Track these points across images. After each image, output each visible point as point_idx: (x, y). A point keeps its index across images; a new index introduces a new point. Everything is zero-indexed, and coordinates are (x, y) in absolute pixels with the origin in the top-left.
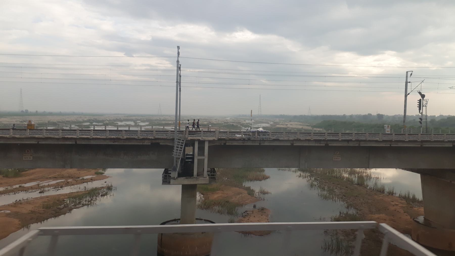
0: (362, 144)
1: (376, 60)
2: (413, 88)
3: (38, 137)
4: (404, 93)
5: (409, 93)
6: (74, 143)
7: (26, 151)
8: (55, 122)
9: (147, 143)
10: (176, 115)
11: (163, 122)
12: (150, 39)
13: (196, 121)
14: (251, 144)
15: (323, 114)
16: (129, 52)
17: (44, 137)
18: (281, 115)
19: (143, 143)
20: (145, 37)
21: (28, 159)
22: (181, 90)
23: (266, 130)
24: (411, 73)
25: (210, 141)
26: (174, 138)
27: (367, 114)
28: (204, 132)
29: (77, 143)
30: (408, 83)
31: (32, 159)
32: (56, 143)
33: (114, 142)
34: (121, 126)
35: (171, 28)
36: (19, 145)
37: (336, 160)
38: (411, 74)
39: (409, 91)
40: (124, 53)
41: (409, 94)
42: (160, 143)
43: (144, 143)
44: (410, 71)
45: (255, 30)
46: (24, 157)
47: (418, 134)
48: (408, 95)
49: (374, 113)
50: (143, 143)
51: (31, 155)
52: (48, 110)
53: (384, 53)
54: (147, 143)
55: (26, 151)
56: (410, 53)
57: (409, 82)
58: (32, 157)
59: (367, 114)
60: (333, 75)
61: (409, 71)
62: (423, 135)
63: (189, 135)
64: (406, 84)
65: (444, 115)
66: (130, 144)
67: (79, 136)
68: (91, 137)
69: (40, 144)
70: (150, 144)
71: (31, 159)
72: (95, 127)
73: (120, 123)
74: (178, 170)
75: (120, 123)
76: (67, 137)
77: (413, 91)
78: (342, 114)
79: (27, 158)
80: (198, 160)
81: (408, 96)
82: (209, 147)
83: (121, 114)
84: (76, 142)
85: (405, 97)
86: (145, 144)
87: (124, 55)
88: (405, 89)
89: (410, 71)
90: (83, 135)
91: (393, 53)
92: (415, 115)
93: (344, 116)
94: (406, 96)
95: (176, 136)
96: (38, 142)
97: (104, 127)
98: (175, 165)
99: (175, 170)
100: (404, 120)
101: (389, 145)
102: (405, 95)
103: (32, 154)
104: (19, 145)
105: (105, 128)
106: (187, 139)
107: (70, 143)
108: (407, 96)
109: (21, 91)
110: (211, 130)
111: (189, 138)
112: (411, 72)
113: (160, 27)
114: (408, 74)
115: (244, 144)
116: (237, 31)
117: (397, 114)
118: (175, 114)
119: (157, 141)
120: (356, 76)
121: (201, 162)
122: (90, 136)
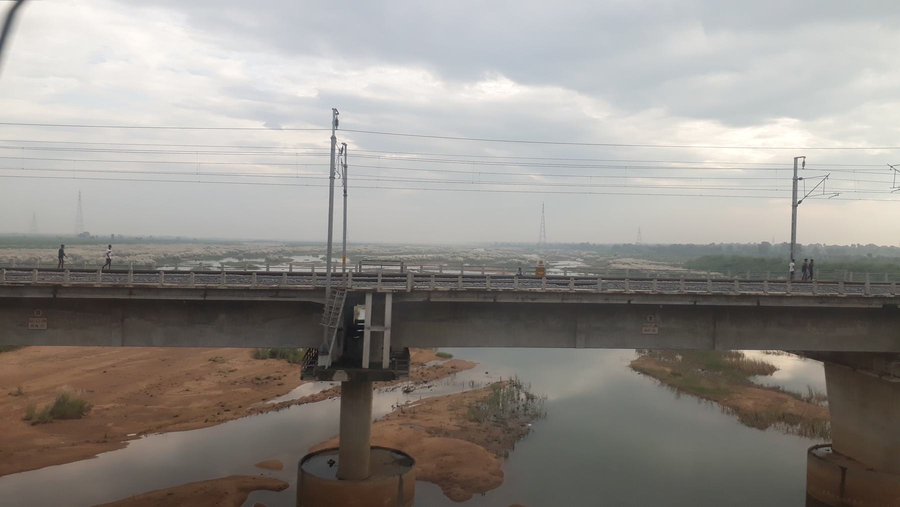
0: (702, 303)
1: (759, 137)
2: (808, 189)
3: (701, 294)
4: (791, 199)
5: (801, 199)
6: (755, 304)
7: (648, 319)
8: (177, 257)
9: (876, 304)
10: (343, 243)
11: (382, 258)
12: (314, 95)
13: (809, 262)
14: (835, 306)
15: (673, 242)
16: (274, 121)
17: (544, 291)
18: (582, 244)
19: (869, 305)
20: (306, 91)
21: (652, 333)
22: (348, 193)
23: (595, 273)
24: (803, 161)
25: (396, 295)
26: (325, 288)
27: (850, 246)
28: (228, 273)
29: (760, 305)
30: (798, 180)
31: (657, 332)
32: (725, 304)
33: (821, 303)
34: (298, 264)
35: (355, 73)
36: (661, 306)
37: (34, 328)
38: (804, 163)
39: (800, 196)
40: (264, 123)
41: (800, 202)
42: (898, 305)
43: (871, 304)
44: (801, 157)
45: (520, 78)
46: (644, 329)
47: (890, 284)
48: (798, 205)
49: (864, 243)
50: (563, 300)
51: (656, 326)
52: (145, 233)
53: (775, 123)
54: (876, 304)
55: (648, 319)
56: (828, 121)
57: (801, 179)
58: (657, 329)
59: (850, 246)
60: (674, 165)
61: (799, 157)
62: (670, 282)
63: (355, 283)
64: (794, 182)
65: (708, 244)
66: (847, 306)
67: (769, 292)
68: (625, 291)
69: (498, 303)
70: (881, 307)
71: (44, 329)
72: (315, 267)
73: (297, 259)
74: (330, 352)
75: (297, 259)
76: (749, 294)
77: (810, 195)
78: (759, 242)
79: (649, 330)
80: (372, 333)
81: (799, 207)
82: (393, 305)
83: (195, 241)
84: (758, 303)
85: (793, 208)
86: (873, 306)
87: (264, 125)
88: (793, 192)
89: (801, 157)
90: (752, 289)
91: (794, 121)
92: (851, 244)
93: (765, 246)
94: (795, 206)
95: (328, 284)
96: (629, 301)
97: (354, 267)
98: (326, 341)
99: (325, 353)
100: (792, 254)
101: (626, 302)
102: (793, 203)
103: (657, 324)
104: (661, 306)
105: (268, 268)
106: (349, 290)
107: (749, 304)
108: (797, 206)
109: (80, 196)
110: (485, 273)
111: (355, 288)
112: (803, 158)
113: (335, 73)
114: (798, 164)
115: (133, 297)
116: (483, 79)
117: (814, 244)
118: (327, 241)
119: (893, 302)
120: (719, 167)
121: (377, 338)
122: (624, 290)
